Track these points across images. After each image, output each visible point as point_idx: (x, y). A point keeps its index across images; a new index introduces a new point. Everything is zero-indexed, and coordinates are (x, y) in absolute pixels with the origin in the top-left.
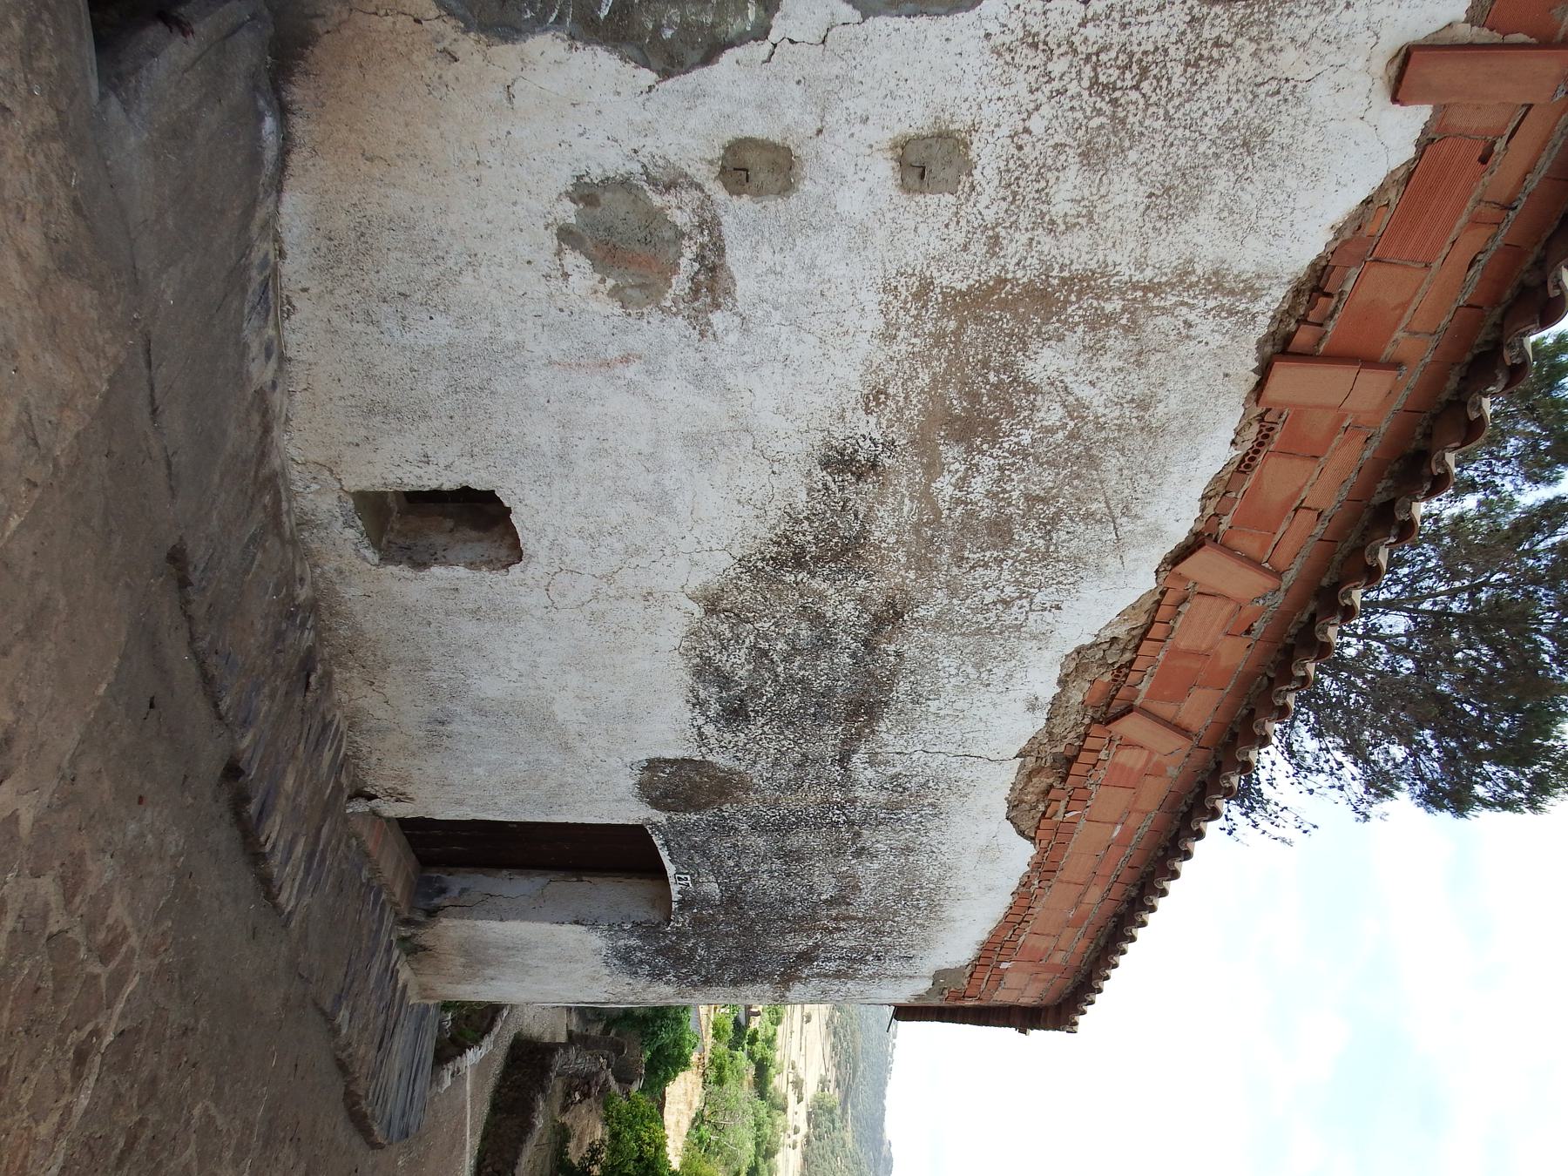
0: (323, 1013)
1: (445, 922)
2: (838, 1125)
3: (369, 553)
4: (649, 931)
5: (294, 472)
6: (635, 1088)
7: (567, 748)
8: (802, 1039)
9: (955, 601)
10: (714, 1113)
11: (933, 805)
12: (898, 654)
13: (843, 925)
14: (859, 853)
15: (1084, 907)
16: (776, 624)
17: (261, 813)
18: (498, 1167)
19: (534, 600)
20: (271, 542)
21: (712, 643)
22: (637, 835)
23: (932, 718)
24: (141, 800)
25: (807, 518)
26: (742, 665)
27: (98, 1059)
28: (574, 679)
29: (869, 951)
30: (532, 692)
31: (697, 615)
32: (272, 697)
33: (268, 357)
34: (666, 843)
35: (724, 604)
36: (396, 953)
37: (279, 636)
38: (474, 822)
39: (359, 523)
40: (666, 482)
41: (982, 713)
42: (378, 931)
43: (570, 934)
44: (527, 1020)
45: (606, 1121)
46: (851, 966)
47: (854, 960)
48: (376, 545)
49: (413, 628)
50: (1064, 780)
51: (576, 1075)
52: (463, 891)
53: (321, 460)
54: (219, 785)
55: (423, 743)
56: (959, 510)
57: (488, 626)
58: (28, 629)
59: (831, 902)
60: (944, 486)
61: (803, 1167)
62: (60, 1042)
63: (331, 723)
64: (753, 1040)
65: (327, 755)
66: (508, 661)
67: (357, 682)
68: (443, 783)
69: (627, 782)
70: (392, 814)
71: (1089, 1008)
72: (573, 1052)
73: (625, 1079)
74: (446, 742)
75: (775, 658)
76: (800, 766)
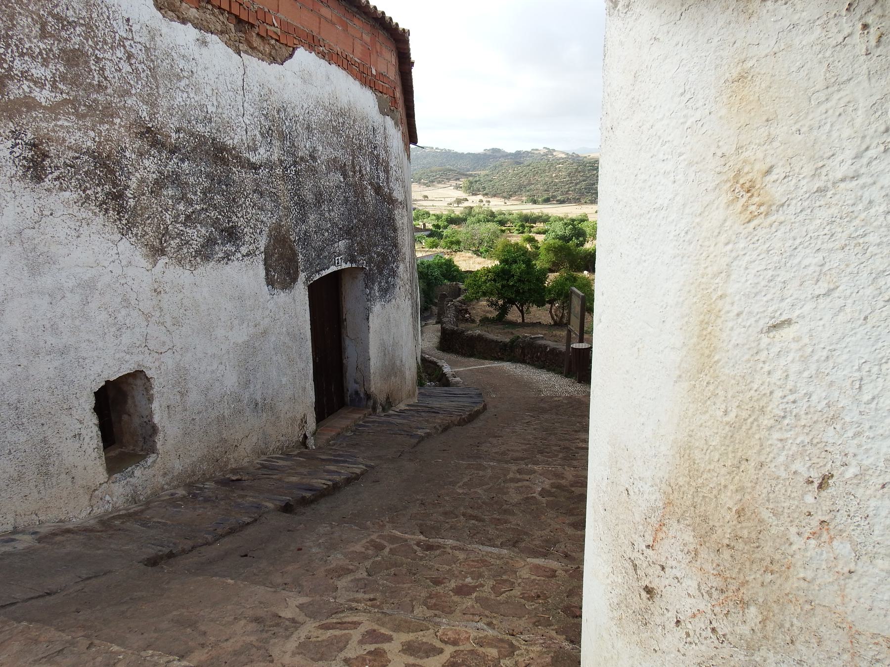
0: (419, 442)
1: (373, 389)
2: (477, 179)
3: (150, 460)
4: (369, 279)
5: (98, 511)
6: (462, 286)
7: (265, 333)
8: (437, 199)
9: (133, 92)
10: (474, 245)
11: (278, 112)
12: (178, 131)
13: (357, 168)
14: (314, 158)
15: (334, 20)
16: (167, 210)
17: (311, 490)
19: (169, 361)
20: (147, 515)
21: (185, 250)
22: (314, 289)
23: (220, 110)
24: (300, 549)
25: (84, 191)
26: (198, 231)
27: (431, 540)
28: (220, 332)
29: (372, 153)
30: (231, 356)
31: (167, 260)
32: (243, 497)
33: (13, 540)
34: (318, 272)
35: (156, 243)
36: (391, 412)
37: (207, 500)
38: (315, 380)
39: (129, 469)
40: (70, 285)
41: (213, 77)
42: (379, 422)
43: (375, 322)
44: (431, 345)
45: (478, 299)
46: (381, 164)
47: (378, 162)
48: (144, 458)
49: (197, 428)
50: (253, 26)
51: (457, 317)
52: (356, 382)
53: (88, 497)
54: (296, 514)
55: (270, 413)
56: (61, 86)
57: (190, 385)
58: (190, 626)
59: (345, 176)
60: (43, 96)
61: (498, 197)
62: (421, 559)
63: (261, 464)
64: (437, 226)
65: (281, 463)
66: (212, 372)
67: (236, 455)
68: (293, 399)
69: (282, 297)
70: (314, 424)
71: (394, 21)
72: (445, 320)
73: (459, 292)
74: (268, 401)
75: (190, 210)
76: (261, 194)
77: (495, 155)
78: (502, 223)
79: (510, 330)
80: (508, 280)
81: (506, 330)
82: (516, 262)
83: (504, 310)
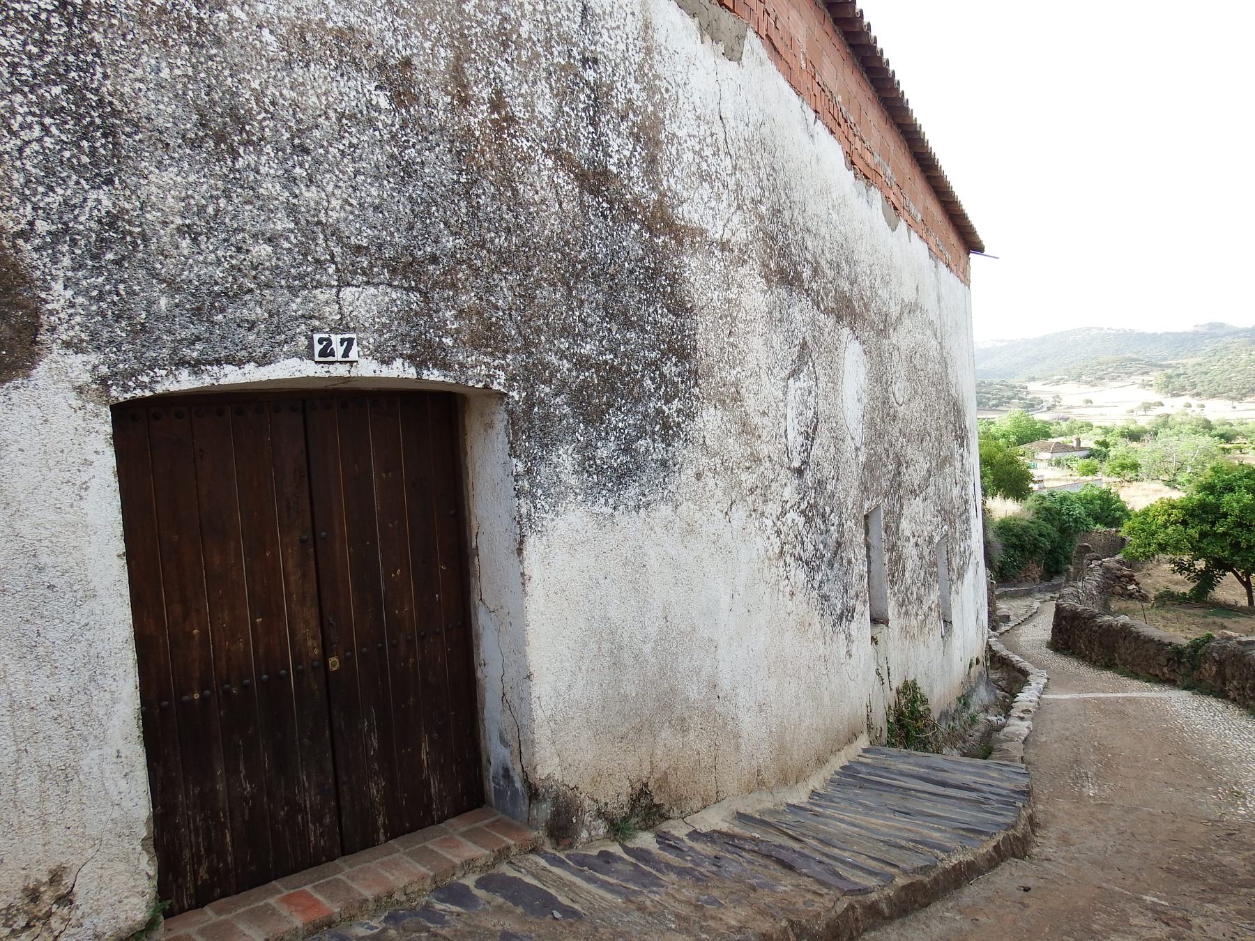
2: (1181, 371)
10: (1167, 471)
18: (1162, 660)
34: (196, 366)
52: (504, 742)
61: (1221, 398)
77: (1214, 332)
78: (1226, 437)
79: (1219, 620)
80: (1213, 524)
81: (1210, 620)
82: (1231, 490)
83: (1206, 581)
